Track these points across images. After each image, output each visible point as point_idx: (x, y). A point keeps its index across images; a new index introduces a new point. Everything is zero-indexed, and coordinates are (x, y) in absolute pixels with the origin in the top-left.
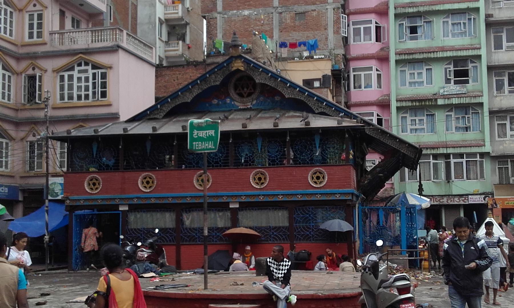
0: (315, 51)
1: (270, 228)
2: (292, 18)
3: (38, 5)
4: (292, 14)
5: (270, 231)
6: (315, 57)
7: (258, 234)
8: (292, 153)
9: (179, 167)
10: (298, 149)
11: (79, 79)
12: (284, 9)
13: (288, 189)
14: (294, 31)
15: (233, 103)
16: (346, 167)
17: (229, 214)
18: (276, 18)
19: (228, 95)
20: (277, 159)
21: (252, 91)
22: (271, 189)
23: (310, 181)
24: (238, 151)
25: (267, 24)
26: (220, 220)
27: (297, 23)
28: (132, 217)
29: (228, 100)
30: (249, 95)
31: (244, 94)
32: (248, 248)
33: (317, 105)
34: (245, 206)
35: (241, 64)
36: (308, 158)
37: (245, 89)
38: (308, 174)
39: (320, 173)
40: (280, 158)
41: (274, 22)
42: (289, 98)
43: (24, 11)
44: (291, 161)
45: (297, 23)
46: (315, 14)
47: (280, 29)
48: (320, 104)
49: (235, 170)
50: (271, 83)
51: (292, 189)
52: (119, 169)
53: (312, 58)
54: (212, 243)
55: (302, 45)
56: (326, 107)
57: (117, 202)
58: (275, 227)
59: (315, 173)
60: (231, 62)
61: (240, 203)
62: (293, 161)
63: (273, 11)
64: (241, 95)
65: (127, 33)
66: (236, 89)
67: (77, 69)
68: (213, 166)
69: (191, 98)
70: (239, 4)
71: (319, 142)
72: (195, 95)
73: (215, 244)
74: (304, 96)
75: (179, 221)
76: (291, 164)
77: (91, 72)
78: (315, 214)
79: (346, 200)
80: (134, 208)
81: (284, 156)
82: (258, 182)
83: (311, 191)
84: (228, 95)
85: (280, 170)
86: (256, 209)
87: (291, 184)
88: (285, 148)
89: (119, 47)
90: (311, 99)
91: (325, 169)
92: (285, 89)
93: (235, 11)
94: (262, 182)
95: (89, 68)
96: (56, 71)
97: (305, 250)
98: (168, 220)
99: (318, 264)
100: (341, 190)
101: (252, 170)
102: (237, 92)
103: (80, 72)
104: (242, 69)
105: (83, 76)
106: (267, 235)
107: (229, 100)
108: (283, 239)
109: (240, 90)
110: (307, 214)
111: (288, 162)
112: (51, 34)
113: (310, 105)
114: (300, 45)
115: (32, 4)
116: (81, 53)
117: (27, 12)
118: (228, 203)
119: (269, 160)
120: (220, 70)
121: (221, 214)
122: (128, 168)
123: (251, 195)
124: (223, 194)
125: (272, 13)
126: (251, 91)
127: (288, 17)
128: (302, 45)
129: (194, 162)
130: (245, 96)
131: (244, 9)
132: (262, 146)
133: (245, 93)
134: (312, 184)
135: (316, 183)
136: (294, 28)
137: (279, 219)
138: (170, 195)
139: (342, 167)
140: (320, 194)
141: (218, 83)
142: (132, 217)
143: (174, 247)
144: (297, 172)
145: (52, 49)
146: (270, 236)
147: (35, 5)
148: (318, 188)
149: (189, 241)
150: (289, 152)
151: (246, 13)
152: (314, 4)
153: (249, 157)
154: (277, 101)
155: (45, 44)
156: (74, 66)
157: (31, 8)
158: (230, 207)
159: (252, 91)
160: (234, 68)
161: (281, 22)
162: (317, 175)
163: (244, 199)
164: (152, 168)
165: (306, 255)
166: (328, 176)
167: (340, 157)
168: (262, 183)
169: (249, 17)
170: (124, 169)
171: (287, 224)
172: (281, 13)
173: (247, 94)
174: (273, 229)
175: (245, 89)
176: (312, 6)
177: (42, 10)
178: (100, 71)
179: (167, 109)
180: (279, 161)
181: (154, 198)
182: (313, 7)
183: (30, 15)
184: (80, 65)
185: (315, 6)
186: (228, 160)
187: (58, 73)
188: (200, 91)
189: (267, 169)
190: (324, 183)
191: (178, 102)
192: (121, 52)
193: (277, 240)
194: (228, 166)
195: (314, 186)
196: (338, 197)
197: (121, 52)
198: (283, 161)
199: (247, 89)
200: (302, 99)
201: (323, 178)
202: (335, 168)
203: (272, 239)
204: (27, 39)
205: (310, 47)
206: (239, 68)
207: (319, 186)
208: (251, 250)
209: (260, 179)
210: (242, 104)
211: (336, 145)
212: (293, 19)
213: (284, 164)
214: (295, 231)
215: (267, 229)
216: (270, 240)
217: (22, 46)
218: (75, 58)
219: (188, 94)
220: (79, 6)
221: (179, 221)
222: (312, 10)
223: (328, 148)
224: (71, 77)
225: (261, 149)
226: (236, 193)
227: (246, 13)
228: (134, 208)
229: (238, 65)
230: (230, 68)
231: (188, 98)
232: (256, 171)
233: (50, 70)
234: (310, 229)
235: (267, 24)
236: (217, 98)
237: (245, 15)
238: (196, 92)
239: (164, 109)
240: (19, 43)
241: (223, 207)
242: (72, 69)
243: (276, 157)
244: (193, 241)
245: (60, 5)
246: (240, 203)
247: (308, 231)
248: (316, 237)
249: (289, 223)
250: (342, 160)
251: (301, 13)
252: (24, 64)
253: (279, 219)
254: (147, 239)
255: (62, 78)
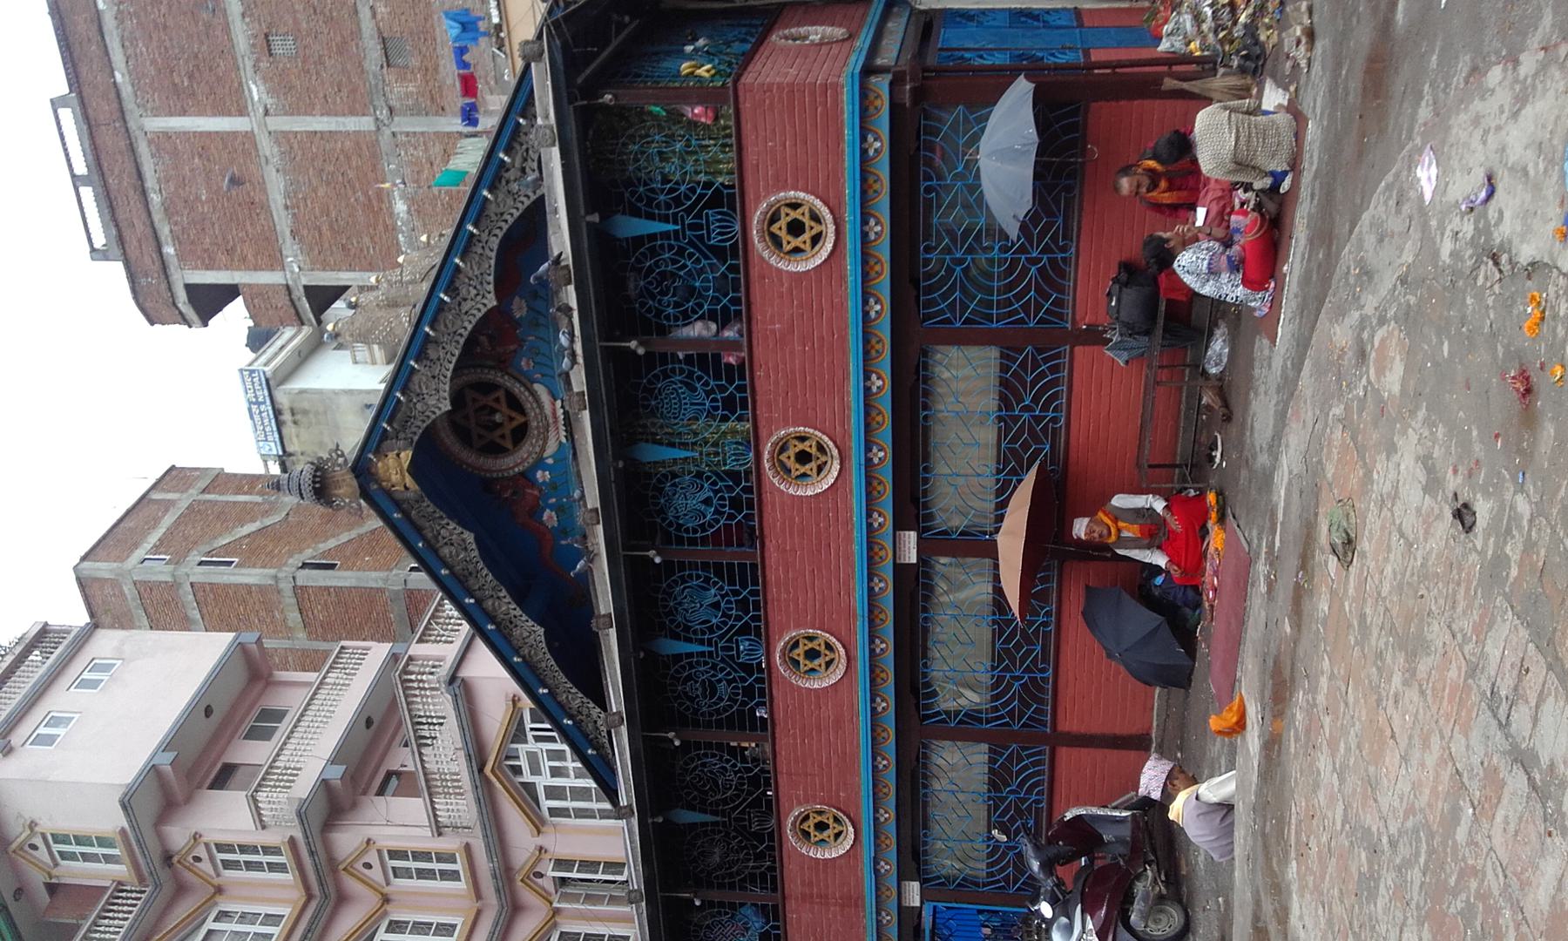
0: (480, 19)
1: (1005, 422)
2: (402, 78)
3: (366, 859)
4: (390, 76)
5: (1016, 419)
6: (496, 20)
7: (1030, 479)
8: (698, 330)
9: (764, 728)
10: (677, 305)
11: (555, 772)
12: (380, 102)
13: (845, 352)
14: (436, 69)
15: (550, 461)
16: (746, 106)
17: (943, 560)
18: (404, 124)
19: (526, 477)
20: (722, 389)
21: (501, 394)
22: (844, 420)
23: (811, 266)
24: (695, 531)
25: (426, 150)
26: (961, 594)
27: (415, 62)
28: (946, 863)
29: (542, 476)
30: (515, 404)
31: (515, 424)
32: (1080, 528)
33: (515, 187)
34: (912, 506)
35: (391, 460)
36: (713, 268)
37: (498, 418)
38: (779, 271)
39: (774, 219)
40: (717, 377)
41: (418, 129)
42: (498, 297)
43: (387, 890)
44: (729, 334)
45: (415, 62)
46: (382, 9)
47: (437, 114)
48: (512, 174)
49: (771, 545)
50: (449, 355)
51: (843, 339)
52: (775, 907)
53: (498, 28)
54: (1052, 627)
55: (466, 57)
56: (520, 151)
57: (891, 918)
58: (1003, 398)
59: (777, 241)
60: (388, 493)
61: (900, 525)
62: (723, 325)
63: (387, 132)
64: (520, 434)
65: (420, 641)
66: (496, 450)
67: (527, 777)
68: (756, 618)
69: (531, 623)
70: (381, 227)
71: (643, 222)
72: (518, 612)
73: (1059, 620)
74: (484, 236)
75: (965, 726)
76: (740, 333)
77: (532, 746)
78: (954, 240)
79: (895, 108)
80: (913, 860)
81: (706, 360)
82: (813, 465)
83: (851, 266)
84: (526, 477)
85: (768, 383)
86: (926, 469)
87: (822, 338)
88: (674, 355)
89: (452, 679)
90: (492, 209)
91: (758, 200)
92: (466, 306)
93: (401, 238)
94: (814, 451)
95: (522, 749)
96: (538, 825)
97: (1109, 295)
98: (960, 769)
99: (1188, 279)
100: (850, 133)
101: (754, 260)
102: (509, 445)
103: (536, 770)
104: (407, 456)
105: (547, 765)
106: (1032, 432)
107: (539, 474)
108: (1055, 369)
109: (503, 437)
110: (950, 271)
111: (733, 346)
112: (439, 830)
113: (517, 214)
114: (466, 65)
115: (366, 871)
116: (481, 770)
117: (388, 884)
118: (900, 569)
119: (725, 419)
120: (419, 530)
121: (942, 586)
122: (771, 878)
123: (868, 494)
124: (858, 589)
125: (394, 134)
126: (503, 399)
127: (399, 90)
128: (466, 57)
129: (743, 680)
130: (520, 419)
131: (391, 214)
132: (672, 445)
133: (511, 419)
134: (824, 254)
135: (816, 239)
136: (430, 71)
137: (966, 379)
138: (865, 762)
139: (747, 127)
140: (864, 222)
141: (469, 537)
142: (946, 863)
143: (1063, 752)
144: (770, 314)
145: (478, 831)
146: (1038, 420)
147: (368, 866)
148: (838, 232)
149: (1041, 701)
150: (690, 342)
151: (400, 207)
152: (356, 12)
153: (716, 492)
154: (530, 308)
155: (468, 848)
156: (522, 784)
157: (376, 874)
158: (914, 560)
159: (501, 394)
160: (409, 480)
161: (416, 111)
162: (783, 234)
163: (885, 518)
164: (769, 808)
165: (1130, 295)
166: (785, 188)
167: (706, 127)
168: (821, 448)
169: (411, 201)
170: (774, 890)
171: (993, 353)
172: (391, 110)
173: (514, 414)
174: (1009, 407)
175: (498, 418)
176: (361, 16)
177: (379, 852)
178: (529, 725)
179: (575, 698)
180: (731, 382)
181: (876, 810)
182: (365, 13)
183: (396, 876)
184: (517, 770)
185: (359, 7)
186: (730, 566)
187: (543, 822)
188: (504, 593)
189: (763, 432)
190: (818, 203)
191: (548, 662)
192: (465, 673)
193: (1055, 396)
194: (754, 566)
195: (829, 246)
196: (880, 144)
197: (465, 673)
198: (729, 365)
199: (493, 411)
200: (495, 243)
201: (795, 206)
202: (751, 157)
203: (1051, 414)
204: (462, 885)
205: (471, 35)
206: (406, 466)
207: (831, 228)
208: (1089, 512)
209: (803, 457)
210: (552, 434)
211: (653, 149)
212: (404, 74)
213: (741, 365)
214: (1021, 321)
215: (1008, 430)
216: (1055, 420)
217: (479, 896)
218: (498, 785)
219: (516, 632)
220: (373, 727)
221: (965, 726)
222: (374, 15)
223: (666, 180)
224: (552, 793)
225: (684, 446)
226: (858, 549)
227: (400, 207)
228: (913, 860)
229: (395, 467)
230: (409, 495)
231: (532, 632)
232: (770, 474)
233: (540, 841)
234: (1015, 262)
235: (426, 150)
236: (535, 511)
237: (409, 212)
238: (506, 605)
239: (576, 704)
240: (471, 905)
241: (913, 589)
242: (530, 788)
243: (712, 391)
244: (1042, 690)
245: (365, 793)
246: (900, 525)
247: (1025, 271)
248: (1054, 239)
249: (989, 343)
250: (716, 118)
251: (385, 48)
252: (527, 896)
253: (966, 379)
254: (1031, 877)
255: (554, 812)
